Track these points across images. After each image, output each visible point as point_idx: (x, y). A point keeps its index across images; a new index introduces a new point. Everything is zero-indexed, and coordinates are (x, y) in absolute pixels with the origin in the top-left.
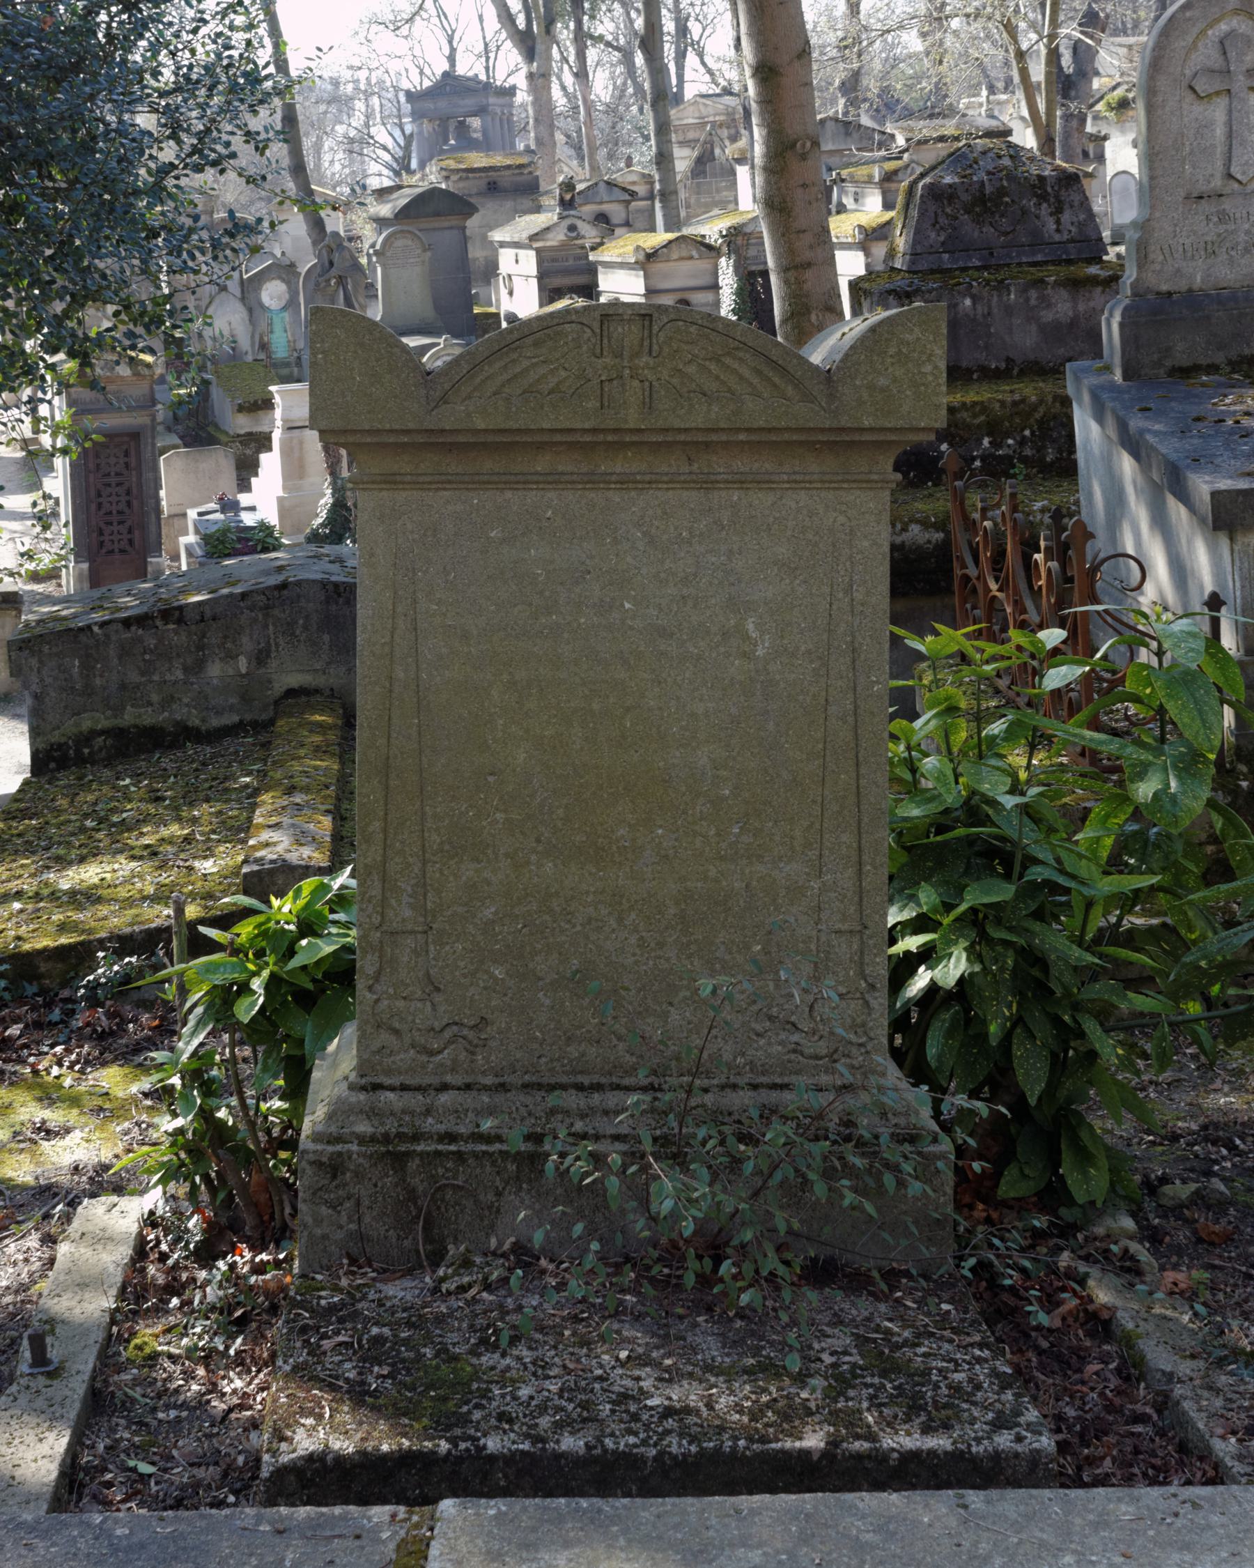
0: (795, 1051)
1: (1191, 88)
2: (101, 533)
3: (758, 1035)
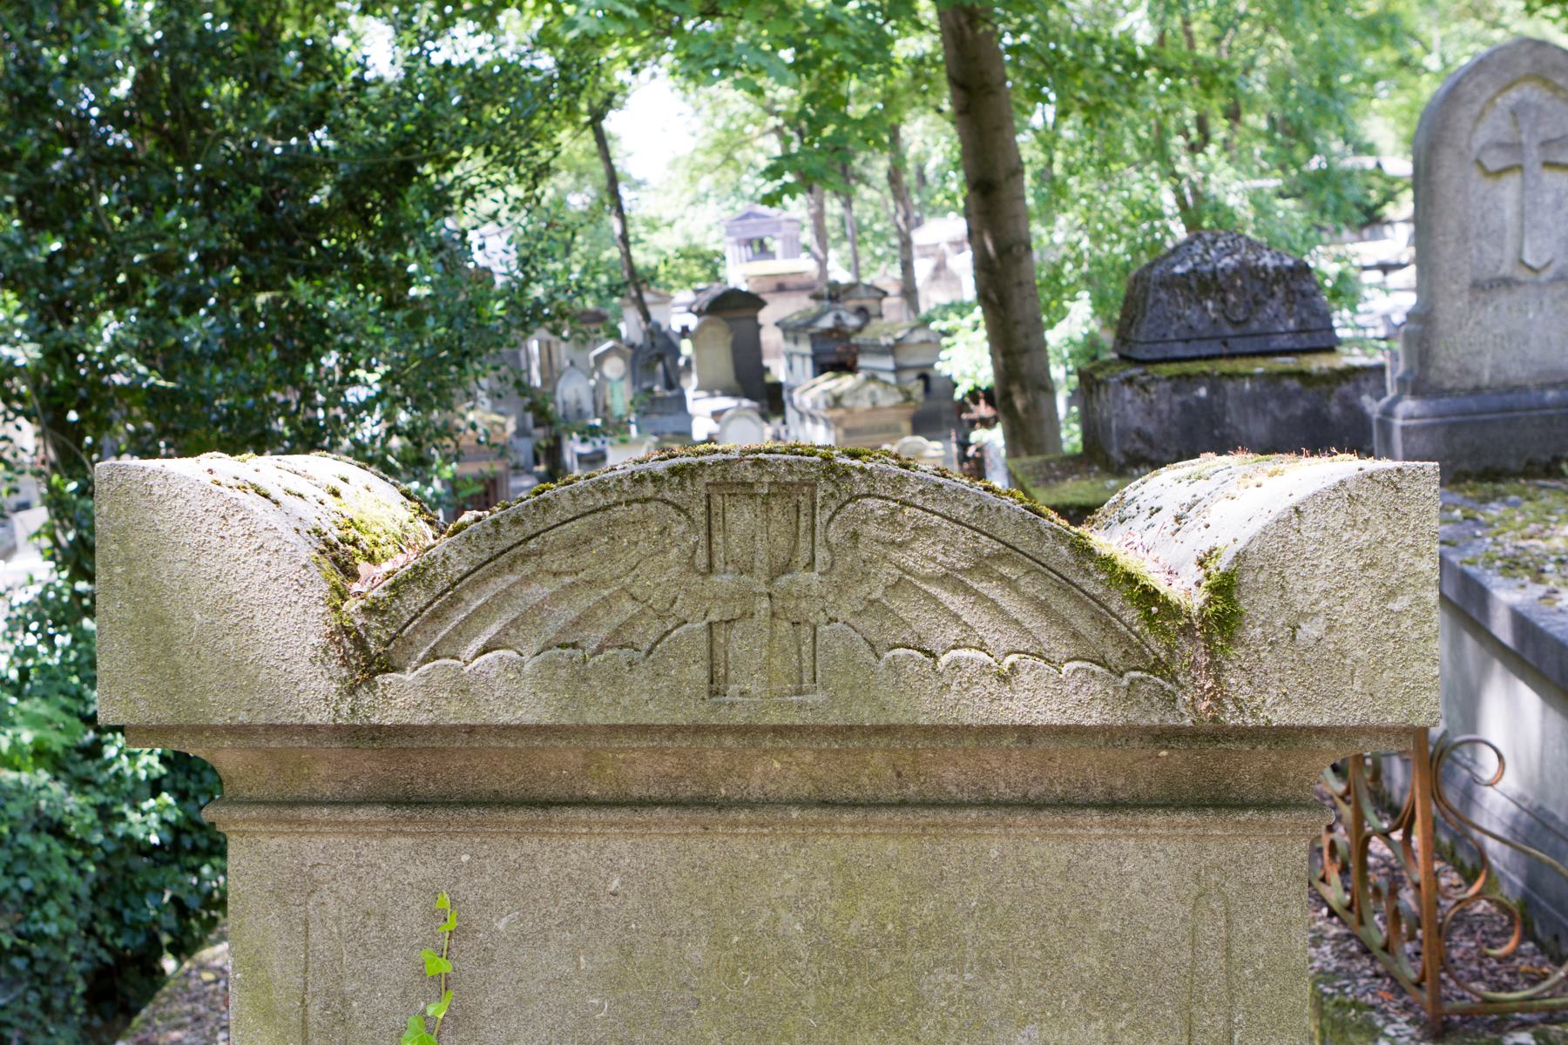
1: (1479, 162)
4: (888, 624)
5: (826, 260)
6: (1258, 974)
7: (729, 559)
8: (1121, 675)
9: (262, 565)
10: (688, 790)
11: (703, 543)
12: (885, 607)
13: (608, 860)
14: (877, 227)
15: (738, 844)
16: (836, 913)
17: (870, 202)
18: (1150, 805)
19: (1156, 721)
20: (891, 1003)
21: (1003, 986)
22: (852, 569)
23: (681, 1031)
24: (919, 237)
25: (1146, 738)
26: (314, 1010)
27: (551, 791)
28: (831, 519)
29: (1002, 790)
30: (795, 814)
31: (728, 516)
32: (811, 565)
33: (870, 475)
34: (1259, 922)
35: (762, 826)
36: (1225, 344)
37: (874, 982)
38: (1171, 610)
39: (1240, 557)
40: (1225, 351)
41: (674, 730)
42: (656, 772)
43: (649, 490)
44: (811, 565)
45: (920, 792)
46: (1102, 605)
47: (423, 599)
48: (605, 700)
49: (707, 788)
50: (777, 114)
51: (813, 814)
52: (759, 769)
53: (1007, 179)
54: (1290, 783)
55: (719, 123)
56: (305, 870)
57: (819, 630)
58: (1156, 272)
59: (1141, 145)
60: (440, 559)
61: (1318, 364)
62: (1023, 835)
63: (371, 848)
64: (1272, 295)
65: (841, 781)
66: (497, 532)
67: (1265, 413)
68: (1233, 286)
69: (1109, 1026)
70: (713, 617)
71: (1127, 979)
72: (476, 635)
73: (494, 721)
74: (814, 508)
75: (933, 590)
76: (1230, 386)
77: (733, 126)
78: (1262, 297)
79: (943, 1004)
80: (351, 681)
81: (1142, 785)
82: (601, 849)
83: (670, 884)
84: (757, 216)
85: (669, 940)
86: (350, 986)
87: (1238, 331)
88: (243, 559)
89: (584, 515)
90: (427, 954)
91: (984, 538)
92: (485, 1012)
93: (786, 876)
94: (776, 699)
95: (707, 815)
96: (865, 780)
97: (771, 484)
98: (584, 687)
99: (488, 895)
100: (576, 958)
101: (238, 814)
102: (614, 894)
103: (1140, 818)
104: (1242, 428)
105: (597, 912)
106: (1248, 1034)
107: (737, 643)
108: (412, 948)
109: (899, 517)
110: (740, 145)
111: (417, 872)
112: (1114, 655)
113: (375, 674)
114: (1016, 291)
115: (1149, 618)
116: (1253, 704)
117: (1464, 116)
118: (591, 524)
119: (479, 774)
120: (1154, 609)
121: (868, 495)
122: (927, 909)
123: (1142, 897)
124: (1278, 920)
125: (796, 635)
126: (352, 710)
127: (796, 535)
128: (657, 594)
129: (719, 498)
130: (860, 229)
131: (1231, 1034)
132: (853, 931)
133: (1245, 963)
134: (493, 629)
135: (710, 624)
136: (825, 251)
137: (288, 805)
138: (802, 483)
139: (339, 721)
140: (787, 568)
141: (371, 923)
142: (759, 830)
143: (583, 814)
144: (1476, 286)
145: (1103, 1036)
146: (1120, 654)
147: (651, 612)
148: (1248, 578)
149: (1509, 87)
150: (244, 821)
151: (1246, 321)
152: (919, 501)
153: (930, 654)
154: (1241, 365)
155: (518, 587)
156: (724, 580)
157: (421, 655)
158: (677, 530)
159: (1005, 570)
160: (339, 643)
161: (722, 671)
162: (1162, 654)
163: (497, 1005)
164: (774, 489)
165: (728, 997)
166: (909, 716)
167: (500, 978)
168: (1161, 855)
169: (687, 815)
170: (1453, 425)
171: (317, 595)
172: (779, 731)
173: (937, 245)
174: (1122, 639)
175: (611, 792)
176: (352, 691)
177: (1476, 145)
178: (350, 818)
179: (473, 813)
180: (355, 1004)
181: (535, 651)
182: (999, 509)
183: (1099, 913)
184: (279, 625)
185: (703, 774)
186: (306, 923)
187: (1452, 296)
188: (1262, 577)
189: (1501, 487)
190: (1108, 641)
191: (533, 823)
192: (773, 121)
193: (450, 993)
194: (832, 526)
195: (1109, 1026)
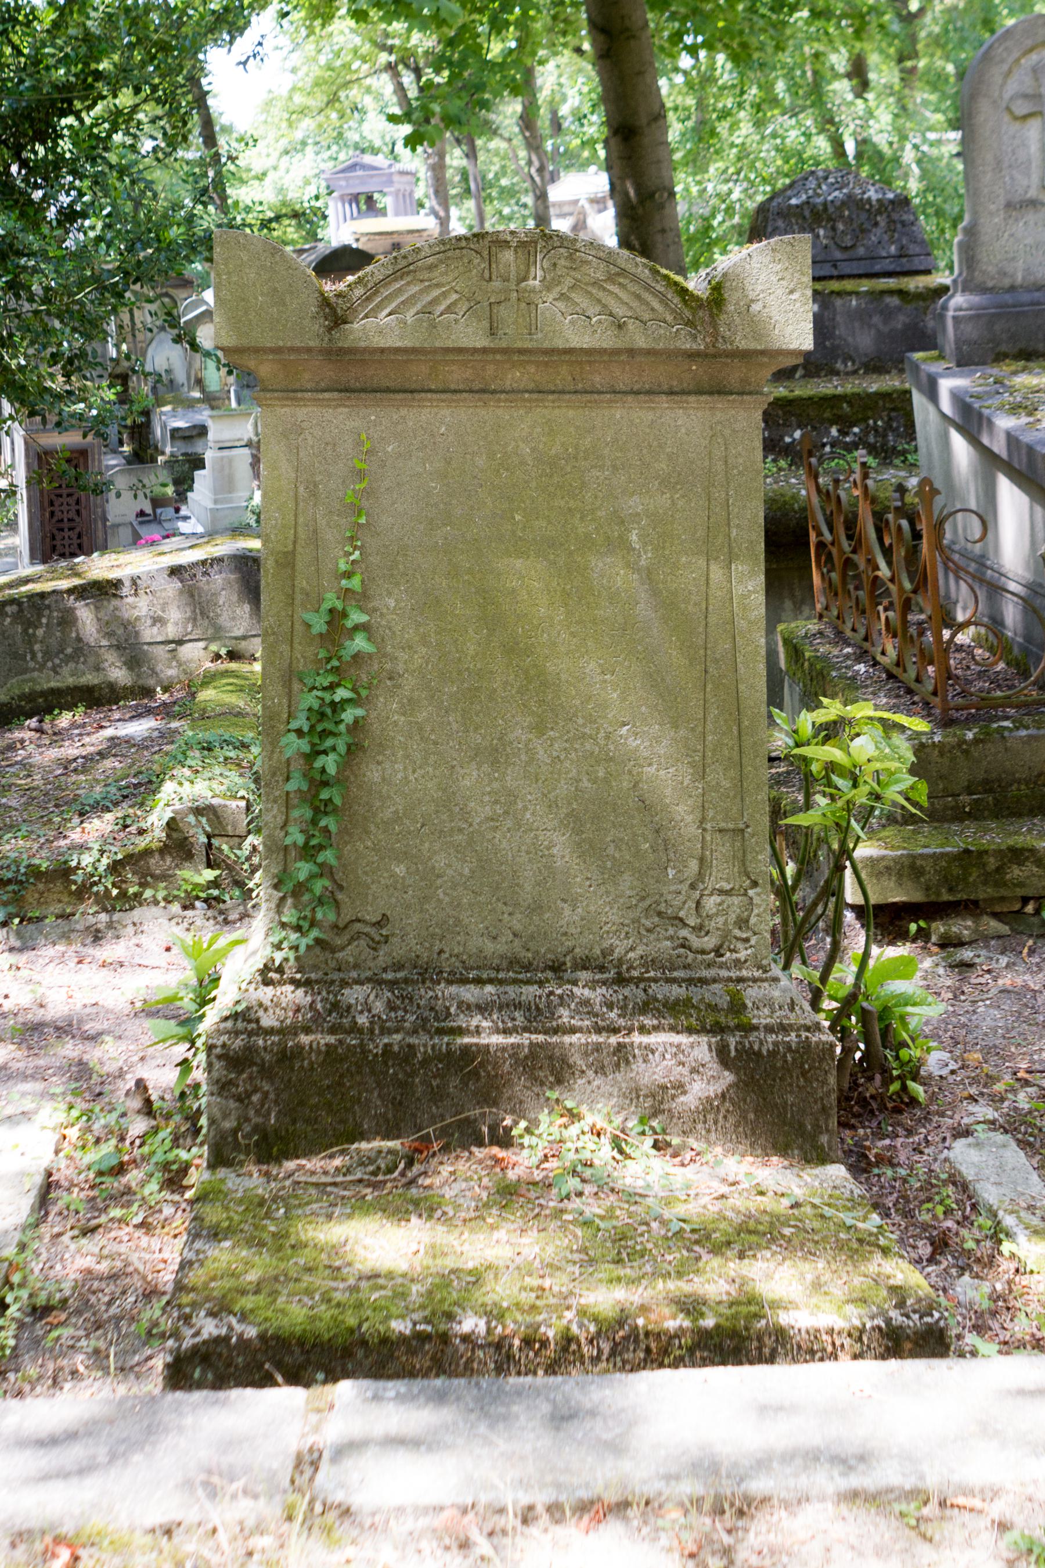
0: (683, 946)
1: (1008, 109)
2: (53, 538)
3: (648, 931)
5: (448, 217)
10: (477, 386)
13: (441, 419)
14: (504, 182)
15: (500, 412)
17: (497, 153)
18: (689, 393)
24: (556, 193)
26: (301, 489)
27: (413, 386)
29: (622, 387)
36: (835, 266)
38: (698, 299)
39: (725, 275)
40: (835, 273)
41: (475, 350)
43: (464, 244)
50: (390, 50)
51: (535, 396)
53: (649, 124)
55: (322, 60)
58: (774, 203)
59: (793, 88)
61: (915, 284)
63: (328, 413)
64: (876, 224)
67: (870, 326)
68: (842, 217)
76: (838, 302)
77: (338, 63)
78: (866, 226)
84: (364, 167)
87: (845, 256)
104: (850, 339)
107: (503, 311)
110: (346, 85)
111: (350, 424)
112: (669, 318)
114: (659, 238)
115: (685, 302)
117: (996, 73)
130: (485, 185)
133: (734, 467)
134: (394, 305)
136: (447, 211)
140: (525, 279)
144: (1009, 205)
149: (1031, 50)
151: (853, 247)
154: (848, 285)
156: (497, 284)
158: (476, 261)
170: (993, 315)
172: (521, 351)
173: (577, 201)
174: (673, 311)
175: (441, 387)
177: (1007, 96)
187: (991, 214)
189: (1031, 364)
192: (384, 58)
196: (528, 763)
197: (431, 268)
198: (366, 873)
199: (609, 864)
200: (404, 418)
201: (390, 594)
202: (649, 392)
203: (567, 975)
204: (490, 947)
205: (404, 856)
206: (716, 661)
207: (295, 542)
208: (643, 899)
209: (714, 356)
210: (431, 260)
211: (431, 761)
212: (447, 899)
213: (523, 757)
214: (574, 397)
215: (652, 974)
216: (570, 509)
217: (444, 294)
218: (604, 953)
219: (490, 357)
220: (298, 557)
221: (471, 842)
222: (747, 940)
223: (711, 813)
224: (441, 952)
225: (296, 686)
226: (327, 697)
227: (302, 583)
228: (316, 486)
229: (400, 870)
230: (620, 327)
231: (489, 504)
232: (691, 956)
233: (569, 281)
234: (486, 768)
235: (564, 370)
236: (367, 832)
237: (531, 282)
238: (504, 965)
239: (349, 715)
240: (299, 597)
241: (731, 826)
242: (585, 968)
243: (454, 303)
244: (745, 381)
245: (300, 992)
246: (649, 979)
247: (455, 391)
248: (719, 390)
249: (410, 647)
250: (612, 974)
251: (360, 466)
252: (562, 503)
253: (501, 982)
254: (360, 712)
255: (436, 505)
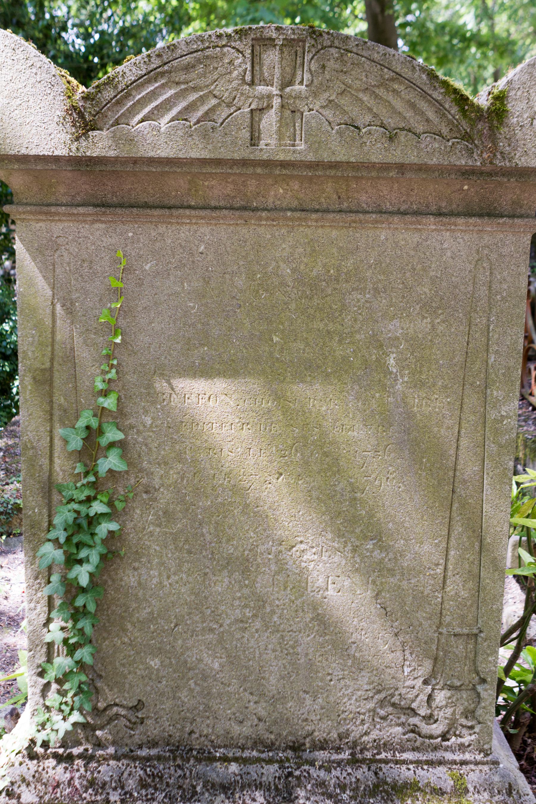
0: (413, 731)
4: (338, 113)
6: (503, 298)
7: (262, 79)
8: (448, 141)
9: (33, 74)
10: (238, 202)
11: (249, 68)
12: (336, 104)
13: (200, 237)
15: (261, 230)
16: (307, 265)
18: (458, 215)
19: (464, 163)
20: (331, 308)
21: (384, 301)
22: (321, 84)
23: (232, 319)
25: (459, 174)
26: (58, 307)
27: (172, 202)
28: (312, 58)
30: (289, 214)
31: (262, 56)
32: (301, 83)
33: (332, 36)
34: (505, 274)
35: (273, 220)
37: (323, 298)
41: (234, 163)
42: (223, 194)
44: (301, 83)
45: (349, 207)
46: (441, 105)
47: (112, 94)
48: (200, 146)
49: (248, 202)
51: (298, 214)
52: (272, 193)
54: (524, 207)
56: (53, 239)
57: (304, 114)
60: (121, 73)
62: (397, 229)
63: (85, 229)
65: (312, 200)
66: (150, 61)
69: (432, 321)
70: (253, 107)
71: (442, 299)
72: (138, 113)
73: (146, 156)
74: (304, 54)
75: (361, 95)
79: (355, 309)
80: (76, 134)
81: (454, 206)
82: (196, 231)
83: (228, 249)
85: (227, 276)
86: (74, 296)
88: (23, 71)
89: (192, 53)
90: (111, 279)
91: (386, 70)
92: (139, 309)
93: (284, 246)
94: (282, 147)
95: (246, 214)
96: (323, 200)
97: (284, 39)
98: (190, 139)
99: (141, 253)
100: (182, 284)
101: (21, 209)
102: (202, 253)
103: (453, 219)
105: (193, 262)
106: (497, 326)
108: (105, 277)
109: (345, 58)
111: (107, 241)
112: (445, 131)
113: (88, 131)
115: (463, 112)
116: (510, 156)
118: (195, 58)
119: (137, 193)
120: (466, 107)
121: (331, 46)
122: (350, 263)
123: (451, 260)
124: (514, 273)
125: (294, 118)
126: (77, 148)
127: (295, 67)
128: (226, 94)
129: (258, 47)
131: (489, 326)
132: (314, 273)
135: (252, 110)
137: (45, 207)
138: (299, 40)
139: (71, 154)
140: (290, 83)
141: (85, 265)
142: (271, 222)
143: (187, 212)
145: (429, 326)
146: (448, 130)
147: (224, 105)
148: (512, 93)
150: (24, 213)
152: (355, 50)
153: (357, 128)
155: (159, 90)
157: (111, 122)
158: (237, 62)
159: (396, 86)
160: (71, 115)
161: (257, 134)
162: (468, 130)
163: (144, 305)
164: (285, 43)
165: (254, 304)
166: (346, 157)
167: (146, 293)
168: (461, 240)
169: (237, 213)
171: (60, 90)
172: (284, 164)
174: (450, 122)
175: (201, 203)
176: (77, 139)
178: (75, 212)
179: (135, 210)
180: (77, 304)
181: (166, 122)
182: (394, 55)
183: (430, 267)
184: (41, 105)
185: (245, 195)
186: (54, 265)
188: (519, 93)
190: (443, 124)
191: (163, 215)
193: (123, 297)
194: (313, 62)
195: (432, 321)
196: (277, 573)
197: (188, 68)
198: (123, 665)
199: (350, 663)
200: (162, 235)
201: (146, 412)
202: (416, 213)
203: (306, 755)
204: (236, 729)
205: (159, 651)
206: (465, 481)
207: (52, 360)
208: (379, 692)
209: (490, 174)
210: (188, 59)
211: (185, 569)
212: (198, 689)
213: (273, 567)
214: (338, 216)
215: (383, 756)
216: (328, 332)
217: (202, 100)
218: (340, 737)
219: (250, 170)
220: (56, 375)
221: (221, 641)
222: (472, 728)
223: (448, 619)
224: (192, 732)
225: (56, 497)
226: (83, 509)
227: (59, 399)
228: (72, 304)
229: (155, 663)
230: (391, 139)
231: (248, 325)
232: (420, 740)
233: (338, 86)
234: (237, 575)
235: (329, 187)
236: (125, 630)
237: (297, 87)
238: (249, 744)
239: (104, 528)
240: (57, 413)
241: (466, 631)
242: (322, 748)
243: (213, 110)
244: (516, 203)
245: (60, 769)
246: (381, 761)
247: (216, 208)
248: (488, 212)
249: (166, 464)
250: (345, 755)
251: (116, 284)
252: (321, 326)
253: (245, 761)
254: (113, 526)
255: (193, 325)
